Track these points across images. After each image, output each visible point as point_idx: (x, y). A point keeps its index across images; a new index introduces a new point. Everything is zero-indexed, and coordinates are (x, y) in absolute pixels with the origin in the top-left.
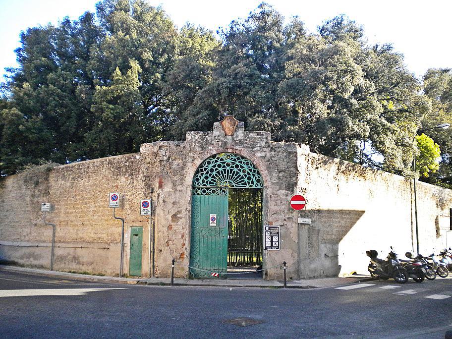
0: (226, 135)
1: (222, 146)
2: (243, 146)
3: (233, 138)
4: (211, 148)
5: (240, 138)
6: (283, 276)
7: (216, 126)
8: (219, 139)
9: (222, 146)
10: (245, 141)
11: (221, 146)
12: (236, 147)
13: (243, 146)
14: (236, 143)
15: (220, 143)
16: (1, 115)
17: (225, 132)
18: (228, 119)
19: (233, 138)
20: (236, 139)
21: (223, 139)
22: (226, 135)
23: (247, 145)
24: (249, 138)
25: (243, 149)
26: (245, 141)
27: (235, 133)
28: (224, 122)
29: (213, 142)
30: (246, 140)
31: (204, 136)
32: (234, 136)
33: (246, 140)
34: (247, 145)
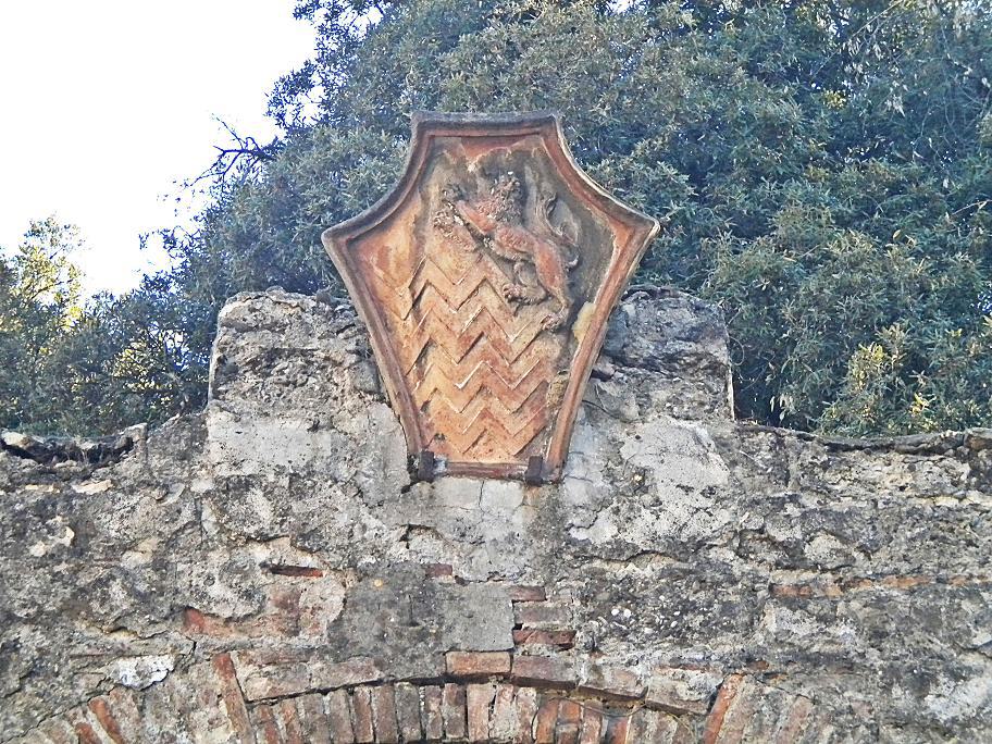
0: (423, 469)
1: (364, 630)
2: (727, 645)
3: (552, 520)
4: (160, 665)
5: (676, 513)
6: (473, 341)
7: (250, 346)
8: (306, 538)
9: (364, 630)
10: (763, 566)
11: (339, 647)
12: (616, 652)
13: (727, 645)
14: (604, 597)
15: (327, 594)
16: (630, 743)
17: (413, 415)
18: (463, 192)
19: (552, 520)
20: (605, 531)
21: (381, 528)
22: (423, 469)
23: (803, 630)
24: (838, 524)
25: (742, 688)
26: (763, 566)
27: (589, 445)
28: (398, 240)
29: (188, 573)
30: (792, 556)
31: (36, 491)
32: (574, 491)
33: (792, 556)
34: (803, 630)
